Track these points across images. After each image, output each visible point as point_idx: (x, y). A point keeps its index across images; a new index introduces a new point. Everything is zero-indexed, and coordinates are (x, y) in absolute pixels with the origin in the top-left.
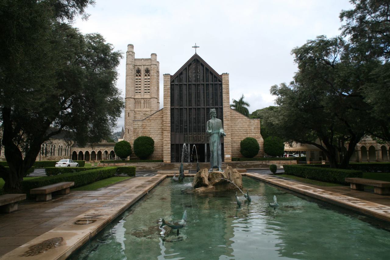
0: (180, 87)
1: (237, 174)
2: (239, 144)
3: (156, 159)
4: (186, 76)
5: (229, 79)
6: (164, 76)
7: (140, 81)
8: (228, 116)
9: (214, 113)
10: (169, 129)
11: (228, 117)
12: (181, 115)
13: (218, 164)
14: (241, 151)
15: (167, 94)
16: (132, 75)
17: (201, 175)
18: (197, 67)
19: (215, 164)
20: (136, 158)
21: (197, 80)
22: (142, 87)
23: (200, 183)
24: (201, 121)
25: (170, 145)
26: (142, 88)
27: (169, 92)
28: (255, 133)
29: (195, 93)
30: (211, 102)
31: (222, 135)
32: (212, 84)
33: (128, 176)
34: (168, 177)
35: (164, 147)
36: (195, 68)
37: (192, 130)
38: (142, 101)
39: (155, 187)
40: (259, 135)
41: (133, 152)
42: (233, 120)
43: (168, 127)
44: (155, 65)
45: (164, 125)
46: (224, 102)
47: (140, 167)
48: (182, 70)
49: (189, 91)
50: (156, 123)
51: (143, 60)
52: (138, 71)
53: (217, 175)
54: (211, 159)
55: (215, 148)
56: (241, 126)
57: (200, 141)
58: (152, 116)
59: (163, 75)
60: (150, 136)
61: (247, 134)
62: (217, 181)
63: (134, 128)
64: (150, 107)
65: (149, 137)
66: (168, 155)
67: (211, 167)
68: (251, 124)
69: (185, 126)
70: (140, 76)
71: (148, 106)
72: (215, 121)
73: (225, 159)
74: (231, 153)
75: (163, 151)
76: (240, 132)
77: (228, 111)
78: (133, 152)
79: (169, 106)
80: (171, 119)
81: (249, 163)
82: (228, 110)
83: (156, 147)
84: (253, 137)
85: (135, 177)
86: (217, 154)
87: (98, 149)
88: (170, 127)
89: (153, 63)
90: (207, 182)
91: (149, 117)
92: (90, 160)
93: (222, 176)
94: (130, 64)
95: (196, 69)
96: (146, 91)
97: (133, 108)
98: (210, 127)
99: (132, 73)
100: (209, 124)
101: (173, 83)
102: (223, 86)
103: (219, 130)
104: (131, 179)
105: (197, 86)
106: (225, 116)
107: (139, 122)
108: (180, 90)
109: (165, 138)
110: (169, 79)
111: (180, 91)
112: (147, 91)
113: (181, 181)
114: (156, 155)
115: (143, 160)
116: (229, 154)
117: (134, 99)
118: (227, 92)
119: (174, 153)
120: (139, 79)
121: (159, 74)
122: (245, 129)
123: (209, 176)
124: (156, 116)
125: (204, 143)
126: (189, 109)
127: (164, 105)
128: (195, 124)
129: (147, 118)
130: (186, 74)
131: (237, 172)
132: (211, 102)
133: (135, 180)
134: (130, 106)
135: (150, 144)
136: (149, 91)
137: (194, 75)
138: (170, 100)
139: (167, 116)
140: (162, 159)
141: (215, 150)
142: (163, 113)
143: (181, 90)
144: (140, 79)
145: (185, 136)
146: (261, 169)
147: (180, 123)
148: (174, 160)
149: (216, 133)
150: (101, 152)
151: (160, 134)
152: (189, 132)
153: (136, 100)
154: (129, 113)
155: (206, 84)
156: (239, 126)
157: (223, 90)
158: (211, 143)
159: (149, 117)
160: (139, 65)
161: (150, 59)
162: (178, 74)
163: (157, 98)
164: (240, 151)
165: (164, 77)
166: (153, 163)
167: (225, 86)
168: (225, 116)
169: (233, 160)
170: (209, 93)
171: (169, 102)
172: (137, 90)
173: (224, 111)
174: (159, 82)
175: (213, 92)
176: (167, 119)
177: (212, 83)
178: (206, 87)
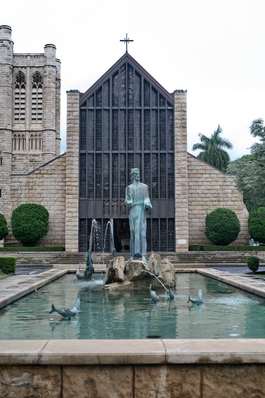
0: (97, 115)
1: (167, 265)
2: (204, 220)
3: (53, 246)
4: (109, 94)
5: (186, 101)
6: (69, 93)
7: (23, 96)
8: (184, 168)
9: (137, 174)
10: (76, 190)
11: (183, 171)
12: (98, 165)
13: (141, 251)
14: (207, 234)
15: (73, 127)
16: (8, 86)
17: (114, 266)
18: (129, 78)
19: (137, 251)
20: (16, 243)
21: (128, 102)
23: (112, 278)
25: (77, 220)
26: (28, 111)
28: (234, 201)
29: (124, 127)
30: (153, 142)
31: (148, 208)
32: (156, 110)
33: (3, 273)
34: (69, 273)
35: (67, 223)
36: (125, 80)
37: (118, 194)
38: (28, 136)
39: (47, 284)
40: (241, 204)
41: (10, 233)
42: (194, 176)
43: (74, 188)
44: (52, 66)
45: (67, 183)
46: (177, 144)
47: (22, 260)
48: (100, 84)
49: (113, 121)
50: (53, 180)
51: (29, 57)
52: (21, 78)
53: (136, 266)
54: (131, 243)
55: (137, 227)
56: (209, 187)
58: (45, 167)
59: (67, 92)
60: (42, 204)
61: (219, 201)
62: (136, 274)
63: (13, 188)
64: (42, 147)
65: (40, 206)
66: (74, 238)
67: (132, 256)
68: (227, 184)
69: (105, 186)
70: (23, 87)
72: (138, 186)
73: (177, 246)
74: (187, 237)
75: (64, 231)
76: (205, 197)
77: (185, 160)
78: (10, 233)
79: (76, 150)
80: (80, 174)
81: (218, 254)
82: (184, 158)
83: (52, 224)
84: (229, 208)
85: (14, 275)
86: (140, 235)
88: (78, 188)
89: (49, 63)
90: (121, 275)
91: (40, 169)
93: (143, 267)
94: (5, 65)
95: (127, 81)
96: (34, 117)
97: (11, 149)
98: (131, 195)
99: (8, 81)
100: (128, 191)
101: (85, 108)
102: (176, 113)
103: (143, 200)
104: (7, 277)
105: (129, 113)
106: (178, 169)
107: (22, 177)
108: (96, 120)
109: (68, 207)
110: (77, 99)
111: (96, 123)
112: (38, 117)
113: (89, 277)
114: (52, 238)
115: (29, 246)
116: (185, 238)
117: (13, 131)
118: (183, 125)
119: (84, 235)
120: (22, 94)
121: (60, 83)
122: (215, 193)
123: (125, 268)
124: (53, 167)
126: (113, 154)
127: (68, 148)
128: (123, 182)
129: (37, 170)
130: (109, 91)
131: (168, 262)
132: (153, 142)
133: (15, 279)
134: (5, 144)
135: (41, 218)
136: (40, 117)
137: (122, 93)
139: (73, 167)
140: (63, 245)
141: (136, 230)
142: (65, 162)
143: (98, 121)
144: (24, 94)
145: (104, 205)
146: (238, 266)
147: (96, 181)
148: (84, 248)
149: (139, 205)
151: (60, 199)
152: (113, 197)
153: (15, 133)
155: (145, 110)
156: (204, 187)
157: (176, 121)
158: (132, 219)
159: (40, 169)
160: (22, 67)
161: (43, 55)
162: (94, 91)
163: (56, 131)
164: (205, 233)
165: (68, 95)
166: (47, 252)
167: (179, 113)
168: (178, 169)
169: (190, 249)
170: (149, 125)
171: (77, 142)
172: (18, 114)
173: (176, 159)
174: (59, 100)
175: (157, 125)
176: (73, 172)
177: (155, 108)
178: (145, 116)
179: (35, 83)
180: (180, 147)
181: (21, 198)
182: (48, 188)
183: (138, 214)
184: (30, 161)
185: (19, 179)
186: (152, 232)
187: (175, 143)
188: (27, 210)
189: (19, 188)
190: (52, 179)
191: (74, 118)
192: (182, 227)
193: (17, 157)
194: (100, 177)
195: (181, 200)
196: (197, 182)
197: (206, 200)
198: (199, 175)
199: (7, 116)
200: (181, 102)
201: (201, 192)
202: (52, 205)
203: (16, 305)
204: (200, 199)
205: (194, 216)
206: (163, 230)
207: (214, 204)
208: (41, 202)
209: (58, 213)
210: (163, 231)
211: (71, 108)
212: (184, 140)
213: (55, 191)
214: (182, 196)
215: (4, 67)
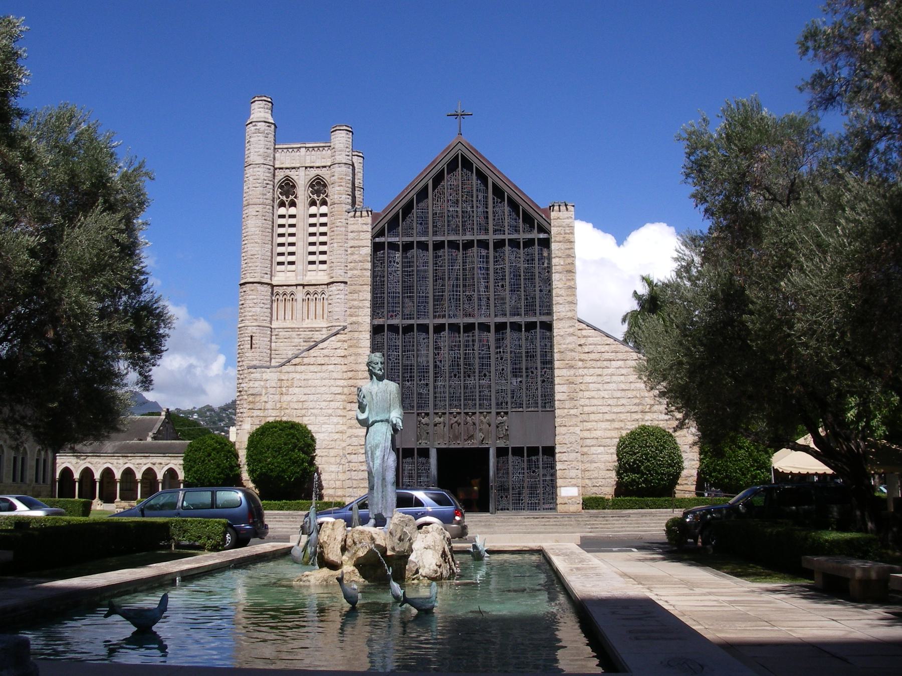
2: (614, 450)
11: (570, 355)
22: (300, 244)
24: (477, 371)
27: (365, 269)
42: (594, 364)
52: (288, 187)
56: (623, 386)
57: (471, 437)
60: (305, 421)
66: (362, 486)
70: (293, 204)
71: (319, 311)
73: (559, 501)
76: (617, 406)
87: (144, 461)
92: (118, 499)
96: (312, 258)
101: (381, 239)
102: (554, 246)
103: (389, 412)
107: (268, 370)
116: (575, 485)
118: (568, 268)
124: (325, 352)
125: (487, 446)
136: (323, 258)
138: (368, 296)
139: (360, 351)
150: (177, 474)
154: (252, 337)
171: (368, 304)
179: (315, 195)
180: (564, 309)
181: (268, 409)
182: (318, 391)
183: (379, 438)
184: (304, 342)
185: (264, 374)
186: (510, 474)
187: (554, 302)
188: (275, 432)
189: (264, 391)
190: (324, 374)
191: (361, 259)
192: (569, 463)
193: (280, 333)
194: (411, 369)
195: (566, 411)
196: (600, 375)
197: (619, 411)
198: (605, 362)
199: (263, 257)
200: (564, 224)
201: (608, 395)
202: (325, 423)
203: (165, 617)
204: (606, 409)
205: (594, 442)
206: (534, 469)
207: (633, 419)
208: (304, 418)
209: (336, 438)
210: (534, 472)
211: (356, 242)
212: (570, 295)
213: (330, 396)
214: (568, 404)
215: (258, 169)
